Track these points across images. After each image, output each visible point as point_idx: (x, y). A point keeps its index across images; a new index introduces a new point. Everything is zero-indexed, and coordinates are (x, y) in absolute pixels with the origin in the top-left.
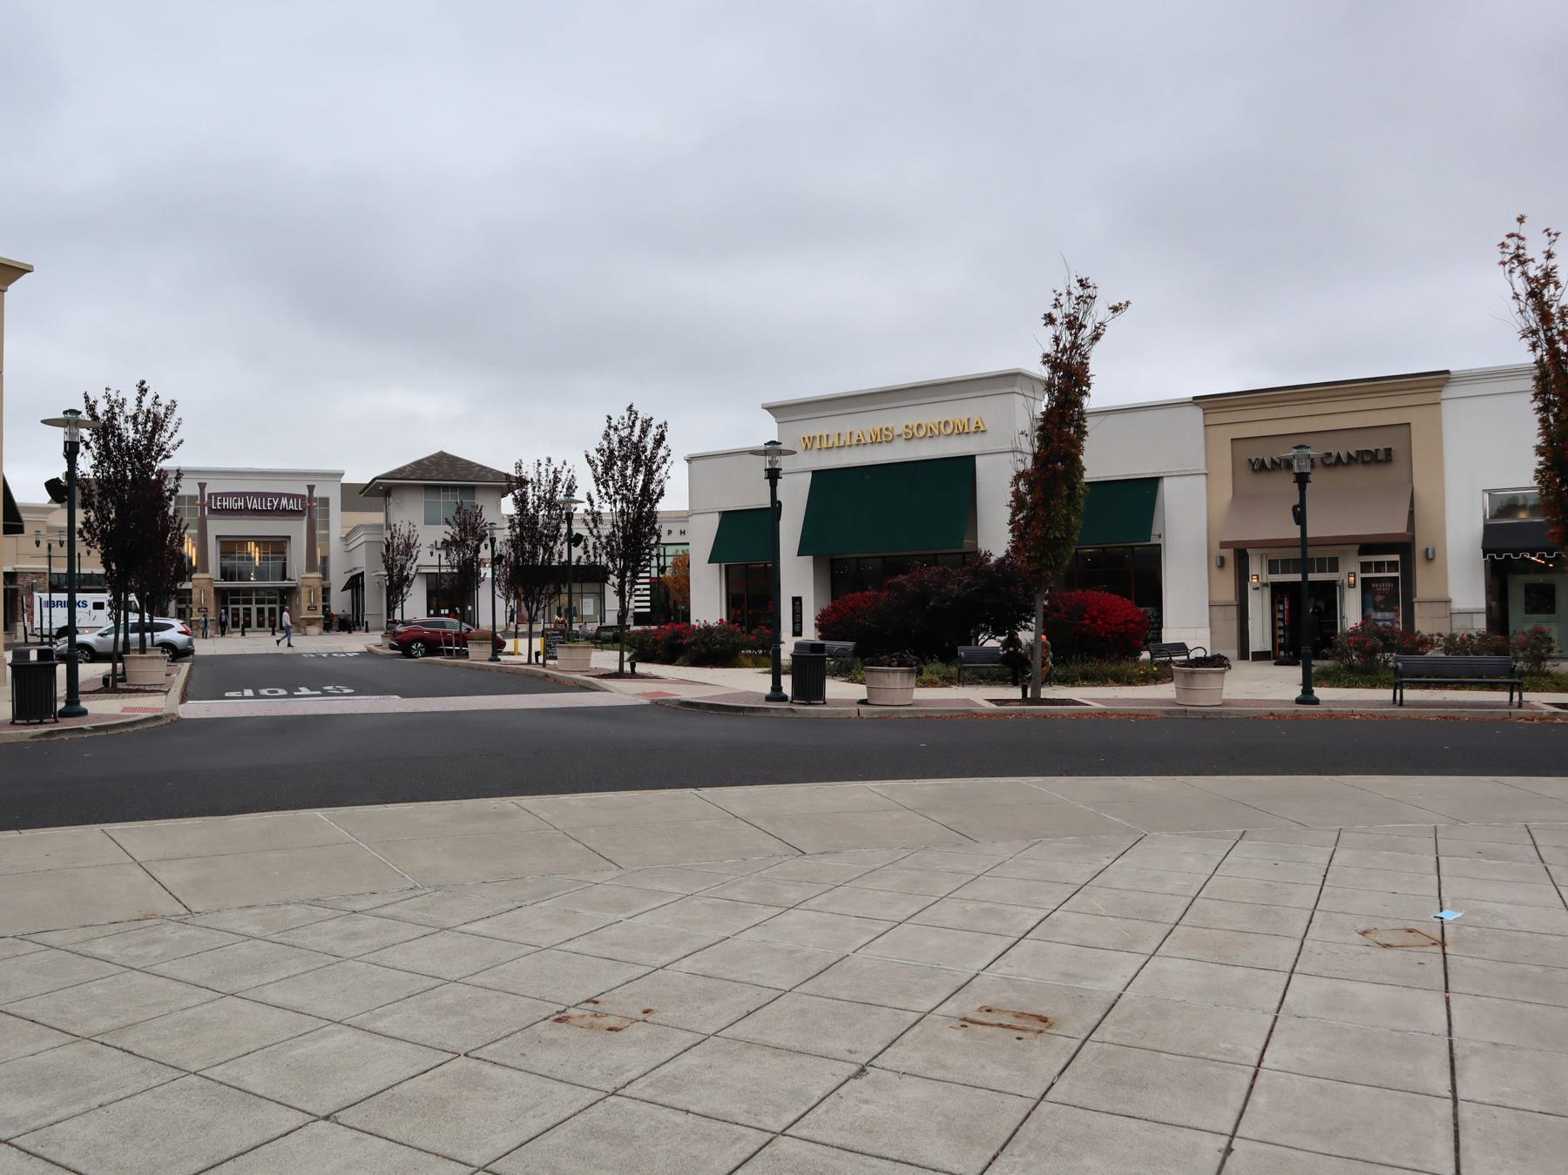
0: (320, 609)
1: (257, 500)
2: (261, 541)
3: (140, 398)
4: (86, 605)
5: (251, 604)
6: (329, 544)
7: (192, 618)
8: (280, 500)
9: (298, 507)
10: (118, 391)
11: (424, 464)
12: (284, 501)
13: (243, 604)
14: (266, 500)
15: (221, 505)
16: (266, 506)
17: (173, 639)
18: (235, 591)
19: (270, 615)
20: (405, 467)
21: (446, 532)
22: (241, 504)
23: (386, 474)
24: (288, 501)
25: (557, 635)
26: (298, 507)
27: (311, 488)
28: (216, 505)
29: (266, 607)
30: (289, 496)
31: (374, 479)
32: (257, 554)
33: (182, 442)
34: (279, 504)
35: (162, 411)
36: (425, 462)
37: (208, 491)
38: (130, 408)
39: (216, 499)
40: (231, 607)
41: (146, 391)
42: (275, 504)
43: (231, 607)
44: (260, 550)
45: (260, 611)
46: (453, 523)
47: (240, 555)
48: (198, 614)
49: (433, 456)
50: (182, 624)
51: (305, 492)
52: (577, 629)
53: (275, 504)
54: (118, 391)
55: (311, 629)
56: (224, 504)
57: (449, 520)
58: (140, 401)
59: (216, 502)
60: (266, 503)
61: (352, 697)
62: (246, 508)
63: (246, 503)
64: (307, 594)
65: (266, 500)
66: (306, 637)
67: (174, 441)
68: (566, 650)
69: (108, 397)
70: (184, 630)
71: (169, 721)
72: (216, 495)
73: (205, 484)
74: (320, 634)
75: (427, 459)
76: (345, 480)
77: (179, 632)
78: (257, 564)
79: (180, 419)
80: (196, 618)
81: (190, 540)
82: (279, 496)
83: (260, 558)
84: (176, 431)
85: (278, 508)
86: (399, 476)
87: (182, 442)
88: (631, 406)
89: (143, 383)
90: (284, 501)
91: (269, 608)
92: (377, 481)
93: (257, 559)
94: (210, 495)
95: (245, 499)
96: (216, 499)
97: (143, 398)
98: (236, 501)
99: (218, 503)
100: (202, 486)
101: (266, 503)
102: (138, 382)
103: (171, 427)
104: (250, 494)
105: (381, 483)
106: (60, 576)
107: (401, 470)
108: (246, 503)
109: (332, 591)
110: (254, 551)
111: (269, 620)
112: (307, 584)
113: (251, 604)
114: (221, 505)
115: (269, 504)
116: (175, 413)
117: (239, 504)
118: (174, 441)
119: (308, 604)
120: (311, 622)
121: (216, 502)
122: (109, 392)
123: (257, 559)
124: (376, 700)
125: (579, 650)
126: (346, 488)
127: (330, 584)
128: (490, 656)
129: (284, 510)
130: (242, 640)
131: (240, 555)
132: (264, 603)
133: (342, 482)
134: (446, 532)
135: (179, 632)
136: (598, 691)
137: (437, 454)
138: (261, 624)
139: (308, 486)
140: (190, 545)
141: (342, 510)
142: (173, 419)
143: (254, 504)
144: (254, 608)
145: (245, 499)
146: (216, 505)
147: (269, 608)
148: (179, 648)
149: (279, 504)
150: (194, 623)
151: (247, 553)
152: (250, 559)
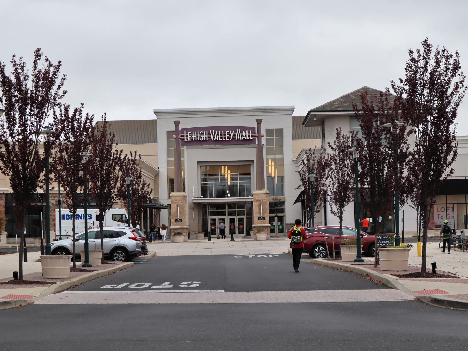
0: (267, 219)
1: (218, 133)
2: (232, 165)
3: (36, 62)
4: (91, 218)
5: (225, 215)
6: (283, 166)
7: (171, 227)
8: (235, 132)
9: (249, 137)
10: (21, 58)
11: (350, 98)
12: (238, 133)
13: (238, 215)
14: (225, 133)
15: (191, 138)
16: (225, 137)
17: (125, 244)
18: (213, 205)
19: (239, 224)
20: (334, 101)
21: (136, 152)
22: (206, 136)
23: (324, 106)
24: (242, 132)
25: (386, 239)
26: (249, 137)
27: (259, 122)
28: (187, 138)
29: (236, 217)
30: (242, 129)
31: (310, 112)
32: (229, 175)
33: (66, 92)
34: (235, 135)
35: (52, 69)
36: (351, 96)
37: (181, 127)
38: (29, 70)
39: (187, 133)
40: (209, 218)
41: (40, 56)
42: (232, 135)
43: (209, 218)
44: (231, 172)
45: (232, 221)
46: (334, 146)
47: (216, 177)
48: (175, 223)
49: (358, 91)
50: (133, 231)
51: (255, 125)
52: (460, 234)
53: (232, 135)
54: (21, 58)
55: (182, 238)
56: (193, 136)
57: (331, 144)
58: (35, 63)
59: (187, 136)
60: (225, 135)
61: (172, 291)
62: (210, 139)
63: (209, 136)
64: (257, 208)
65: (225, 133)
66: (257, 241)
67: (60, 92)
68: (384, 253)
69: (13, 62)
70: (133, 236)
71: (18, 306)
72: (187, 130)
73: (179, 122)
74: (267, 239)
75: (353, 93)
76: (295, 114)
77: (129, 238)
78: (229, 183)
79: (65, 75)
80: (174, 227)
81: (273, 164)
82: (235, 128)
83: (231, 178)
84: (62, 84)
85: (234, 139)
86: (329, 109)
87: (66, 92)
88: (426, 41)
89: (39, 50)
90: (238, 133)
91: (239, 219)
92: (312, 113)
93: (229, 180)
94: (183, 130)
95: (209, 133)
96: (187, 133)
97: (38, 61)
98: (202, 134)
99: (189, 137)
100: (177, 123)
101: (225, 135)
102: (35, 50)
103: (58, 82)
104: (212, 128)
105: (315, 115)
106: (9, 196)
107: (331, 104)
108: (209, 136)
109: (287, 203)
110: (227, 173)
111: (239, 228)
112: (257, 199)
113: (225, 215)
114: (191, 138)
115: (227, 136)
116: (60, 71)
117: (204, 136)
118: (60, 92)
119: (259, 216)
120: (260, 230)
121: (187, 136)
122: (15, 58)
123: (229, 180)
124: (205, 292)
125: (396, 252)
126: (295, 119)
127: (285, 198)
128: (355, 257)
129: (238, 139)
130: (210, 244)
131: (216, 177)
132: (215, 215)
133: (293, 115)
134: (136, 152)
135: (129, 238)
136: (391, 288)
137: (362, 89)
138: (232, 232)
139: (257, 120)
140: (273, 167)
141: (294, 138)
142: (60, 76)
143: (215, 136)
144: (227, 218)
145: (209, 133)
146: (187, 138)
147: (239, 219)
148: (130, 251)
149: (235, 135)
150: (172, 230)
151: (221, 175)
152: (224, 179)
